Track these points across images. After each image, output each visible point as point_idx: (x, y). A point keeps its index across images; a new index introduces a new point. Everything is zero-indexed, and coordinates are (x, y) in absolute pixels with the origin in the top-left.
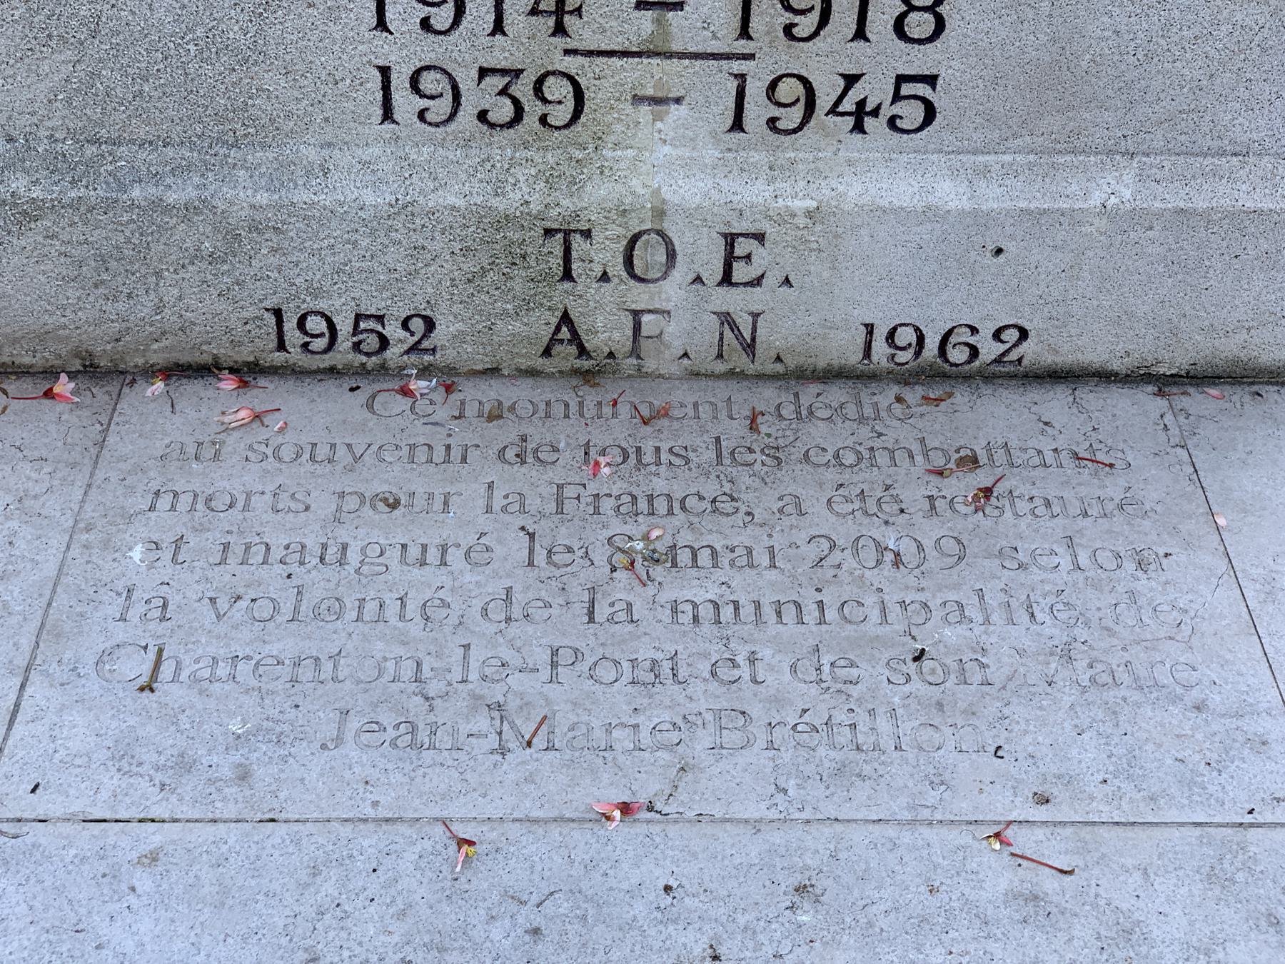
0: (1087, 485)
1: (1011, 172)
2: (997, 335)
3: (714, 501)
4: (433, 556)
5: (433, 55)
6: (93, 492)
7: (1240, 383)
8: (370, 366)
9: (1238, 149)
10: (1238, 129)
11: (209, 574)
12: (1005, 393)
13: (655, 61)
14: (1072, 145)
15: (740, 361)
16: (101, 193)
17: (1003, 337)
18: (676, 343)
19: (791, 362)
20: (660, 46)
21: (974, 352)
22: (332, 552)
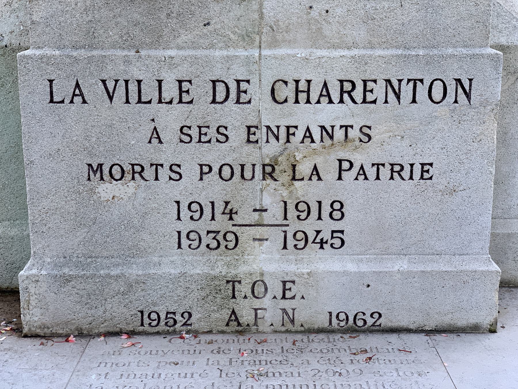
0: (403, 356)
1: (369, 261)
2: (372, 315)
3: (281, 361)
4: (189, 375)
5: (193, 227)
6: (80, 363)
7: (453, 333)
8: (170, 331)
9: (438, 253)
10: (437, 246)
11: (116, 381)
12: (376, 335)
13: (259, 227)
14: (387, 252)
15: (290, 326)
16: (91, 272)
17: (374, 316)
18: (269, 320)
19: (306, 326)
20: (260, 222)
21: (365, 322)
22: (156, 375)
